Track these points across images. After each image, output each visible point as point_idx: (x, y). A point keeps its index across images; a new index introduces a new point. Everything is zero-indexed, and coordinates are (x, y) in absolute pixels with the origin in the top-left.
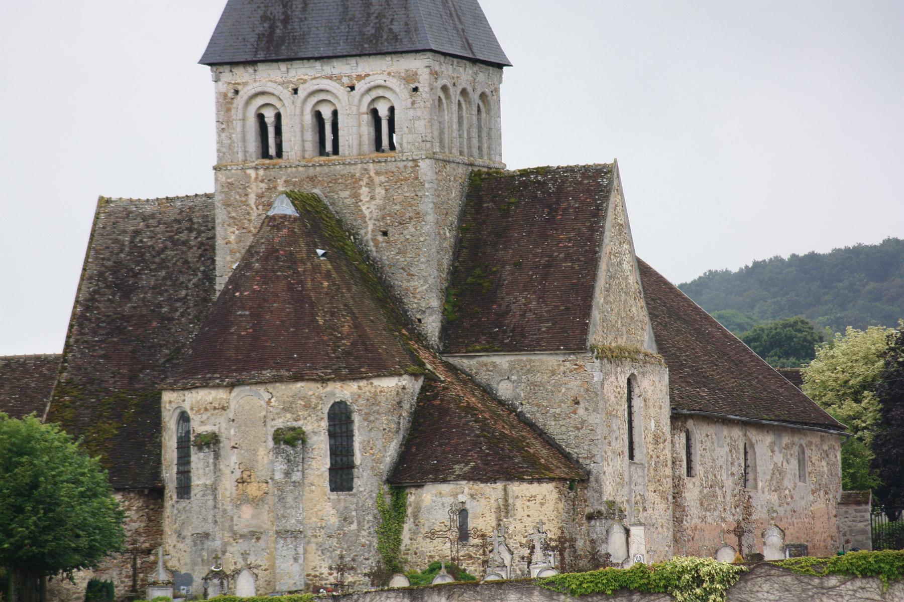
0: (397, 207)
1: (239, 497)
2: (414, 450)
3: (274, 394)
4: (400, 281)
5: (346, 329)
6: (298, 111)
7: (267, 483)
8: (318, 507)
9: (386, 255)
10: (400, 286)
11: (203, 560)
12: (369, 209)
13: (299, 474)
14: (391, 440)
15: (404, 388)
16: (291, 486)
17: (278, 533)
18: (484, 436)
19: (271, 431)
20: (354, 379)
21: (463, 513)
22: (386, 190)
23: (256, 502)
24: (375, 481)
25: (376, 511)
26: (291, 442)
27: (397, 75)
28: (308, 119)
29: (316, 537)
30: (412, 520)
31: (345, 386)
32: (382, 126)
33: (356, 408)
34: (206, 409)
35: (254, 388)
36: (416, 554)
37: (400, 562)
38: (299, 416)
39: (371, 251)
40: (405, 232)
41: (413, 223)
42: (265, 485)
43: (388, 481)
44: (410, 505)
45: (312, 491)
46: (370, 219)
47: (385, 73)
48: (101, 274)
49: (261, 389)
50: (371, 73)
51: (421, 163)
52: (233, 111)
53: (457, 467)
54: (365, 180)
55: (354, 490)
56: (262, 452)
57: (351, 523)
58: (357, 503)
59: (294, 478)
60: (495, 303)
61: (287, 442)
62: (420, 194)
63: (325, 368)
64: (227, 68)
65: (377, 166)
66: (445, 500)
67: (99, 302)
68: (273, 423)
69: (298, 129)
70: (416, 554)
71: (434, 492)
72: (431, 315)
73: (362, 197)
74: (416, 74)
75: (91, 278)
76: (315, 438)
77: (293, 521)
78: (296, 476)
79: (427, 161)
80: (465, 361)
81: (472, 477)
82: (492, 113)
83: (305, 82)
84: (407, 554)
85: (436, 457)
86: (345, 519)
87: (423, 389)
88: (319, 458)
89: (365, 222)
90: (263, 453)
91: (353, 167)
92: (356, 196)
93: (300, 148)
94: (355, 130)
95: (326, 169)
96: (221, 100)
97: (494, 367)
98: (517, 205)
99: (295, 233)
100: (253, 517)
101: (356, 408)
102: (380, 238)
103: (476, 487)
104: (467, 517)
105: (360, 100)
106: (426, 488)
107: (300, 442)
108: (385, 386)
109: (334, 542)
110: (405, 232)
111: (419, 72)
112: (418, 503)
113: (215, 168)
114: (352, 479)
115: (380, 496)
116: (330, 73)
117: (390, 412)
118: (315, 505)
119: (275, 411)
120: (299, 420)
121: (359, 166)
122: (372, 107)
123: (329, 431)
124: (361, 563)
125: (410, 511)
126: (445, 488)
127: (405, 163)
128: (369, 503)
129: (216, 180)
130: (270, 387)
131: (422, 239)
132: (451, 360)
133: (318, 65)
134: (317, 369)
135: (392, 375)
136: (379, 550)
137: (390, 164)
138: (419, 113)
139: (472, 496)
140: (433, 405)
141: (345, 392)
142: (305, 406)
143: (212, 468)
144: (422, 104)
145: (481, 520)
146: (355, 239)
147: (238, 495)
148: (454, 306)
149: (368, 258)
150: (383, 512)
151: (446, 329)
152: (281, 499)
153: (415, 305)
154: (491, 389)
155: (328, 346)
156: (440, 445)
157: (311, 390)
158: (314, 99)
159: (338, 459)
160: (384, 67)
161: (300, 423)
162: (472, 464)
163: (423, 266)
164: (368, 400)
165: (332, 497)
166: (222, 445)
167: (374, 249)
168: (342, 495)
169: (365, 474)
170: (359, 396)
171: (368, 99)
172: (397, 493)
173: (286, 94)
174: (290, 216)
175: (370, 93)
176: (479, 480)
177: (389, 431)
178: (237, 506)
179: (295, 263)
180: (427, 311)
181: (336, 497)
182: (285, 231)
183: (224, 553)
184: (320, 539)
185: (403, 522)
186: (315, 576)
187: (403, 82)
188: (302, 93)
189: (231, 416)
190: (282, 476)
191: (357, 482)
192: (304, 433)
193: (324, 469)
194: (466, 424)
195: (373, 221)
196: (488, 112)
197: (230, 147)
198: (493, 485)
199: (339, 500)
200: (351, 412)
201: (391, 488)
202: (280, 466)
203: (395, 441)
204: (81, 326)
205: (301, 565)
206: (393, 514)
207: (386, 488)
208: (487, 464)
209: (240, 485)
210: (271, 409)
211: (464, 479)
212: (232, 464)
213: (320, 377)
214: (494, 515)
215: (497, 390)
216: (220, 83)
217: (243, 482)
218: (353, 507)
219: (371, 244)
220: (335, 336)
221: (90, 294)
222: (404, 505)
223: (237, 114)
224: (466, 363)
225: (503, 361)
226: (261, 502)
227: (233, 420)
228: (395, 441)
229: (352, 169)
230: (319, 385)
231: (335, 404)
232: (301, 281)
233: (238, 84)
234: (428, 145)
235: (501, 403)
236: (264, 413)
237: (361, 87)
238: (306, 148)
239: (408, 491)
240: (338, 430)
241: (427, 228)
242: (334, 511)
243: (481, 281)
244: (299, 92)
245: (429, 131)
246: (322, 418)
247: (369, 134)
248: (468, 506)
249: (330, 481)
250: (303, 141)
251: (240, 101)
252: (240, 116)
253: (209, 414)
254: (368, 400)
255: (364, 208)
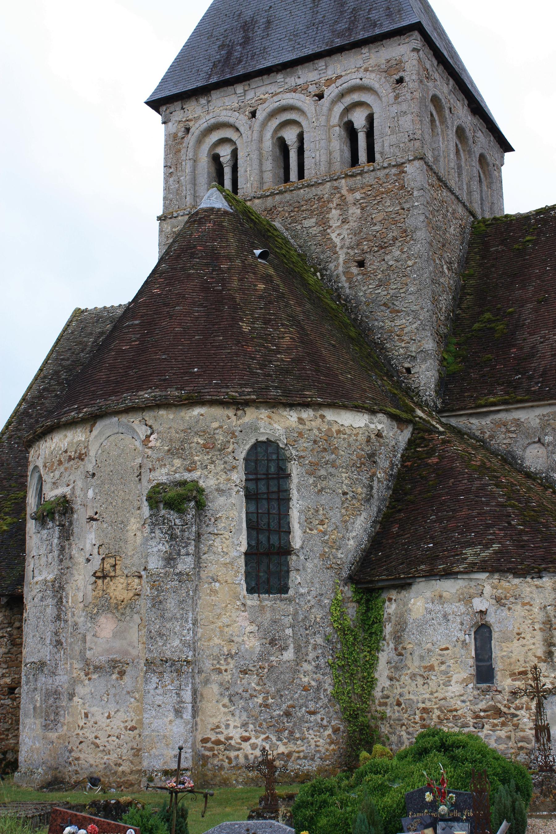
0: (377, 228)
1: (97, 602)
2: (395, 529)
3: (155, 427)
4: (382, 321)
5: (287, 339)
6: (256, 135)
7: (140, 577)
8: (225, 620)
9: (365, 291)
10: (382, 327)
11: (35, 708)
12: (339, 236)
13: (189, 560)
14: (357, 512)
15: (379, 435)
16: (180, 579)
17: (148, 663)
18: (513, 506)
19: (146, 487)
20: (291, 406)
21: (483, 632)
22: (362, 209)
23: (120, 609)
24: (329, 579)
25: (329, 630)
26: (175, 504)
27: (378, 69)
28: (268, 144)
29: (220, 672)
30: (392, 645)
31: (275, 417)
32: (360, 143)
33: (294, 452)
34: (60, 463)
35: (124, 419)
36: (399, 704)
37: (373, 718)
38: (194, 462)
39: (342, 287)
40: (387, 258)
41: (398, 244)
42: (137, 580)
43: (351, 579)
44: (389, 620)
45: (215, 592)
46: (342, 248)
47: (362, 70)
48: (56, 373)
49: (135, 421)
50: (343, 74)
51: (408, 168)
52: (183, 151)
53: (469, 551)
54: (336, 201)
55: (291, 592)
56: (134, 525)
57: (285, 648)
58: (296, 614)
59: (180, 567)
60: (514, 346)
61: (171, 505)
62: (406, 206)
63: (241, 386)
64: (178, 104)
65: (351, 181)
66: (448, 608)
67: (46, 398)
68: (152, 475)
69: (255, 156)
70: (399, 704)
71: (428, 594)
72: (424, 360)
73: (331, 223)
74: (401, 62)
75: (45, 377)
76: (221, 500)
77: (176, 643)
78: (185, 564)
79: (417, 163)
80: (474, 421)
81: (497, 566)
82: (494, 187)
83: (264, 101)
84: (385, 704)
85: (432, 538)
86: (274, 642)
87: (410, 443)
88: (227, 534)
89: (336, 253)
90: (134, 527)
91: (321, 187)
92: (324, 223)
93: (257, 178)
94: (323, 143)
95: (287, 196)
96: (170, 142)
97: (518, 425)
98: (535, 243)
99: (223, 226)
100: (115, 635)
101: (294, 452)
102: (355, 270)
103: (504, 584)
104: (490, 638)
105: (330, 110)
106: (414, 588)
107: (192, 504)
108: (347, 424)
109: (253, 681)
110: (387, 258)
111: (405, 59)
112: (402, 616)
113: (159, 218)
114: (288, 572)
115: (339, 604)
116: (294, 84)
117: (358, 467)
118: (219, 616)
119: (155, 456)
120: (195, 469)
121: (328, 185)
122: (346, 119)
123: (246, 489)
124: (302, 720)
125: (388, 629)
126: (450, 587)
127: (387, 171)
128: (318, 614)
129: (161, 231)
130: (149, 416)
131: (410, 263)
132: (453, 422)
133: (280, 77)
134: (227, 387)
135: (358, 408)
136: (335, 697)
137: (366, 175)
138: (404, 107)
139: (498, 600)
140: (427, 464)
141: (276, 426)
142: (205, 446)
143: (56, 553)
144: (409, 96)
145: (516, 643)
146: (322, 275)
147: (96, 598)
148: (456, 357)
149: (339, 297)
150: (343, 631)
151: (445, 383)
152: (157, 603)
153: (402, 351)
154: (514, 458)
155: (253, 359)
156: (439, 520)
157: (215, 419)
158: (275, 123)
159: (263, 538)
160: (360, 63)
161: (195, 475)
162: (496, 546)
163: (412, 298)
164: (315, 442)
165: (249, 603)
166: (75, 516)
167: (346, 285)
168: (268, 600)
169: (309, 565)
170: (301, 434)
171: (339, 108)
172: (368, 601)
173: (241, 120)
174: (219, 210)
175: (343, 100)
176: (509, 571)
177: (353, 497)
178: (93, 617)
179: (217, 259)
180: (419, 356)
181: (256, 603)
182: (209, 225)
183: (71, 696)
184: (227, 677)
185: (378, 650)
186: (218, 742)
187: (384, 74)
188: (261, 115)
189: (90, 468)
190: (161, 563)
191: (295, 578)
192: (201, 491)
193: (234, 554)
194: (483, 488)
195: (345, 250)
196: (490, 186)
197: (178, 192)
198: (537, 582)
199: (262, 608)
200: (288, 460)
201: (356, 592)
202: (159, 547)
203: (364, 514)
204: (20, 423)
205: (187, 723)
206: (359, 639)
207: (348, 591)
208: (523, 547)
209: (100, 582)
210: (150, 452)
211: (483, 570)
212: (88, 547)
213: (233, 398)
214: (539, 636)
215: (522, 459)
216: (170, 124)
217: (104, 577)
218: (287, 621)
219: (343, 278)
220: (266, 348)
221: (39, 392)
222: (379, 621)
223: (187, 154)
224: (475, 424)
225: (530, 417)
226: (128, 610)
227: (94, 475)
228: (364, 514)
229: (318, 191)
230: (230, 412)
231: (257, 445)
232: (223, 279)
233: (190, 120)
234: (418, 144)
235: (529, 475)
236: (139, 461)
237: (331, 92)
238: (265, 180)
239: (385, 596)
240: (263, 488)
241: (418, 248)
242: (254, 628)
243: (493, 325)
244: (258, 114)
245: (418, 126)
246: (234, 468)
247: (342, 151)
248: (491, 619)
249: (247, 574)
250: (262, 171)
251: (191, 139)
252: (191, 155)
253: (62, 469)
254: (315, 442)
255: (333, 236)
